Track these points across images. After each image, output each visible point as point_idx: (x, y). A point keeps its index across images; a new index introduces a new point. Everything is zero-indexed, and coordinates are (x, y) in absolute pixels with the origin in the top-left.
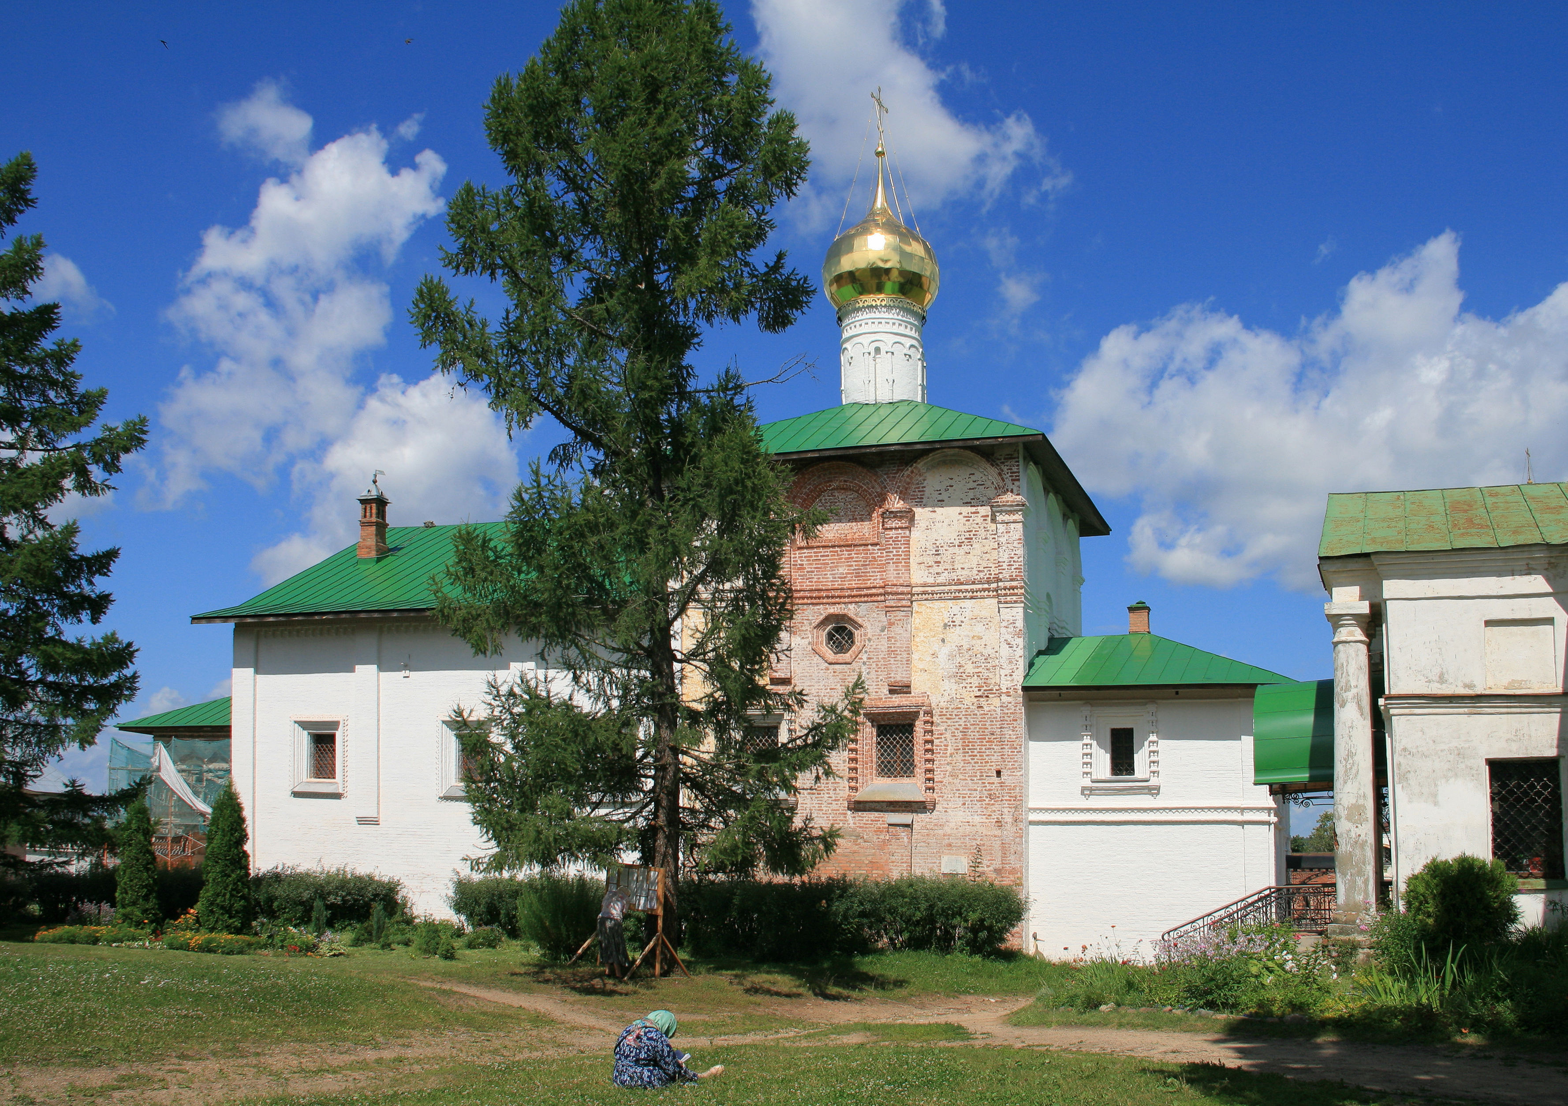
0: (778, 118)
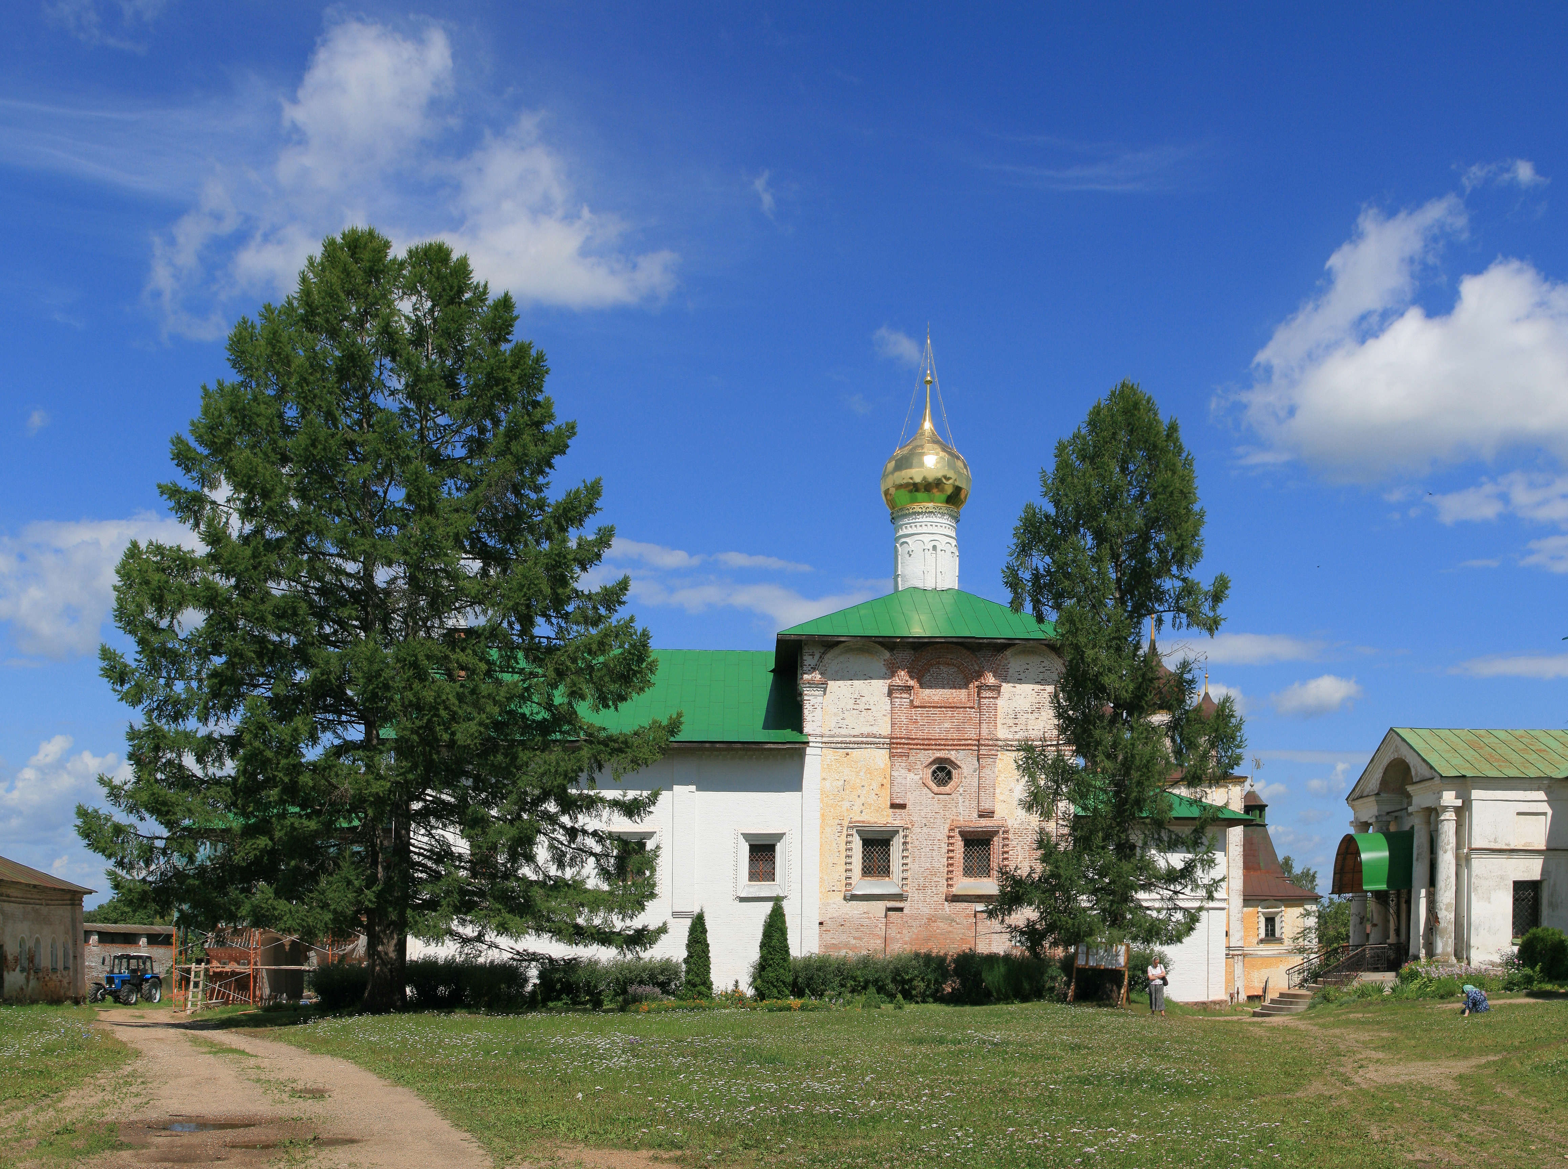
0: (87, 836)
